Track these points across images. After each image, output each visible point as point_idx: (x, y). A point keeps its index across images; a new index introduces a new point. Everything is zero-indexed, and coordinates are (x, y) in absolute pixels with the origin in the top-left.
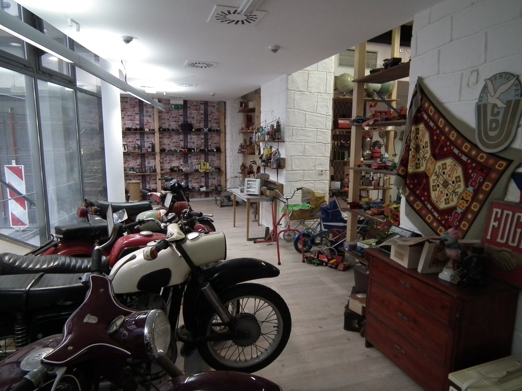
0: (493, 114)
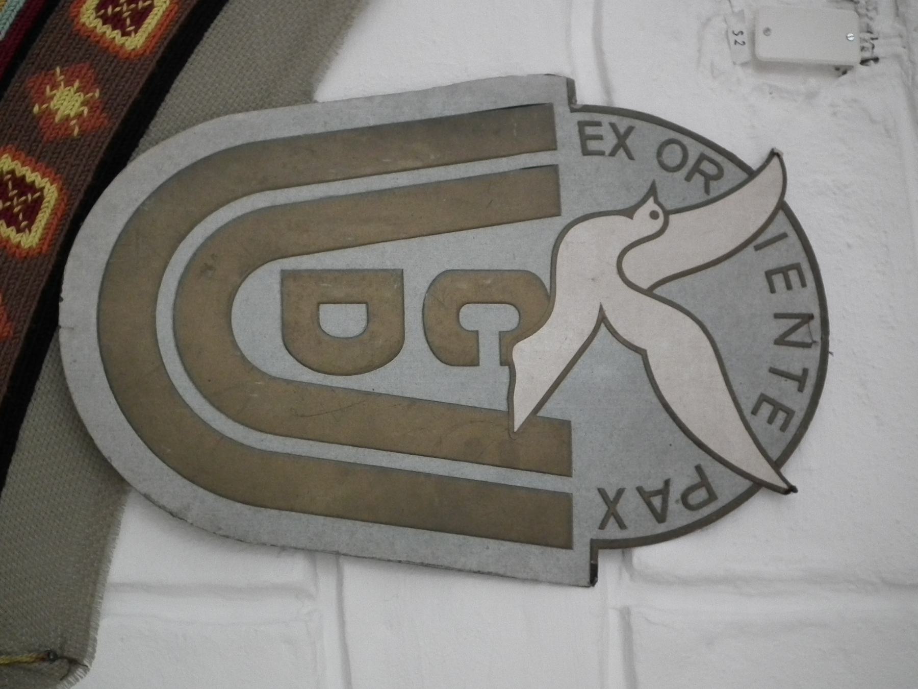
0: (452, 291)
